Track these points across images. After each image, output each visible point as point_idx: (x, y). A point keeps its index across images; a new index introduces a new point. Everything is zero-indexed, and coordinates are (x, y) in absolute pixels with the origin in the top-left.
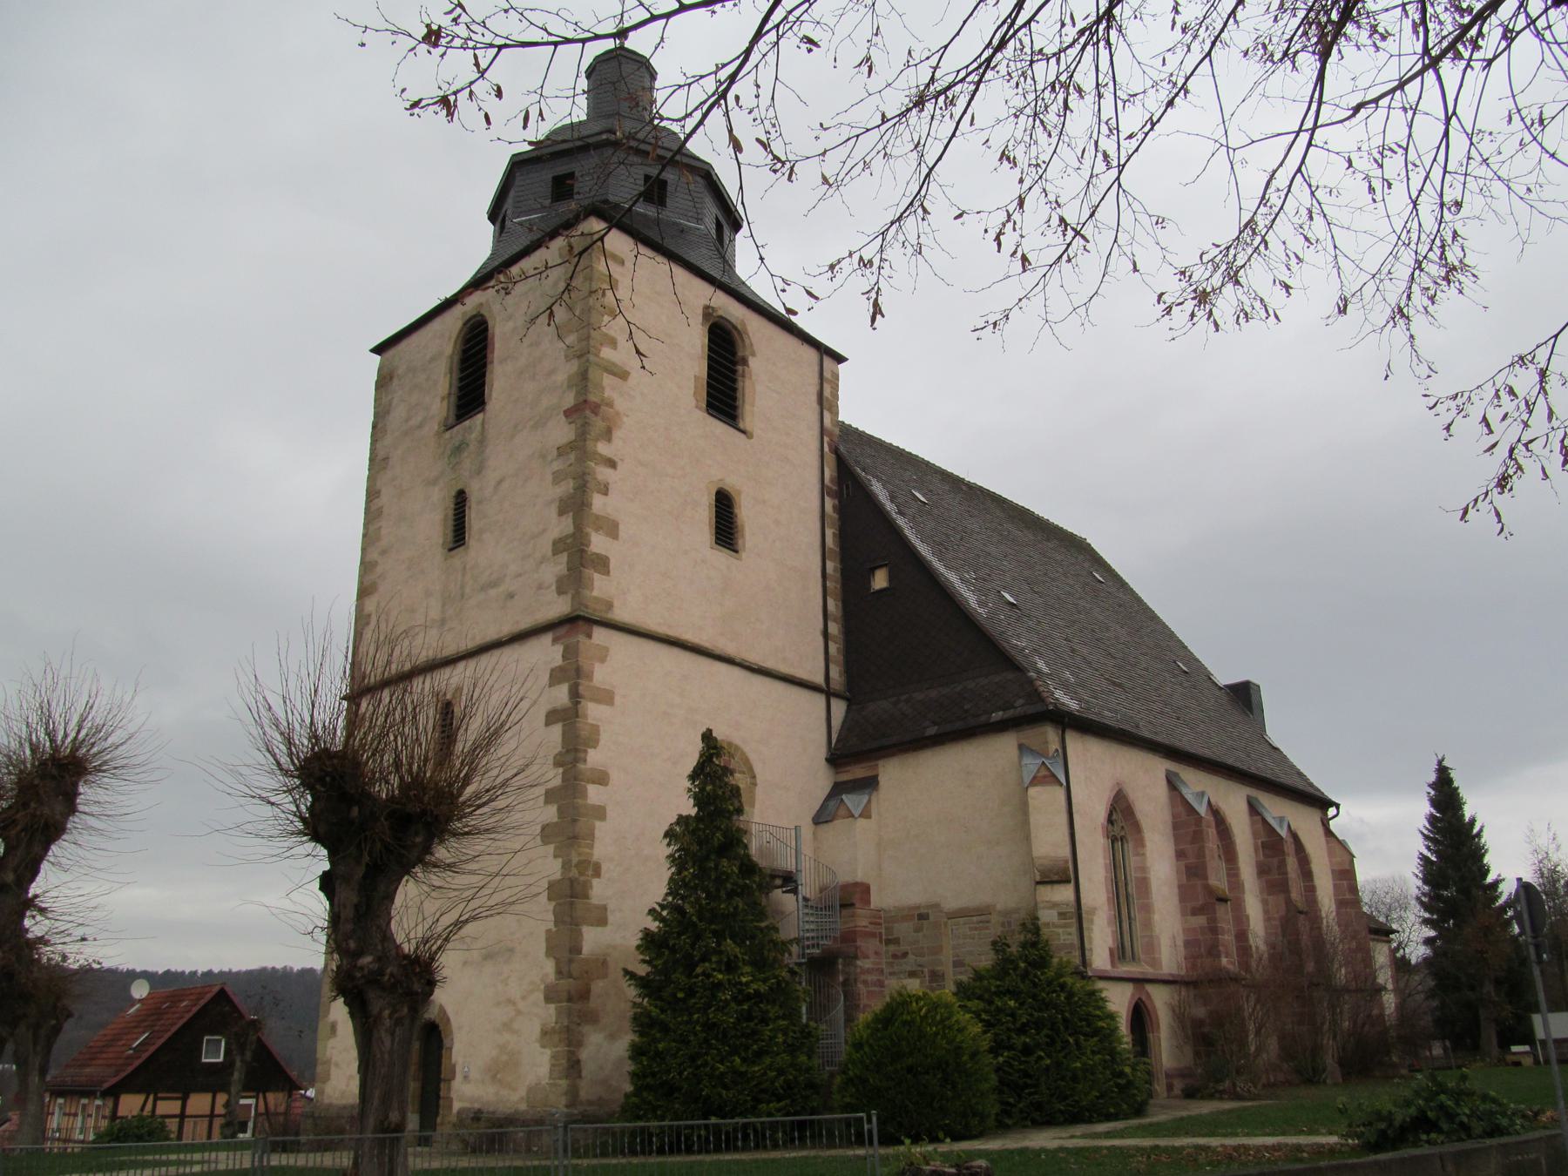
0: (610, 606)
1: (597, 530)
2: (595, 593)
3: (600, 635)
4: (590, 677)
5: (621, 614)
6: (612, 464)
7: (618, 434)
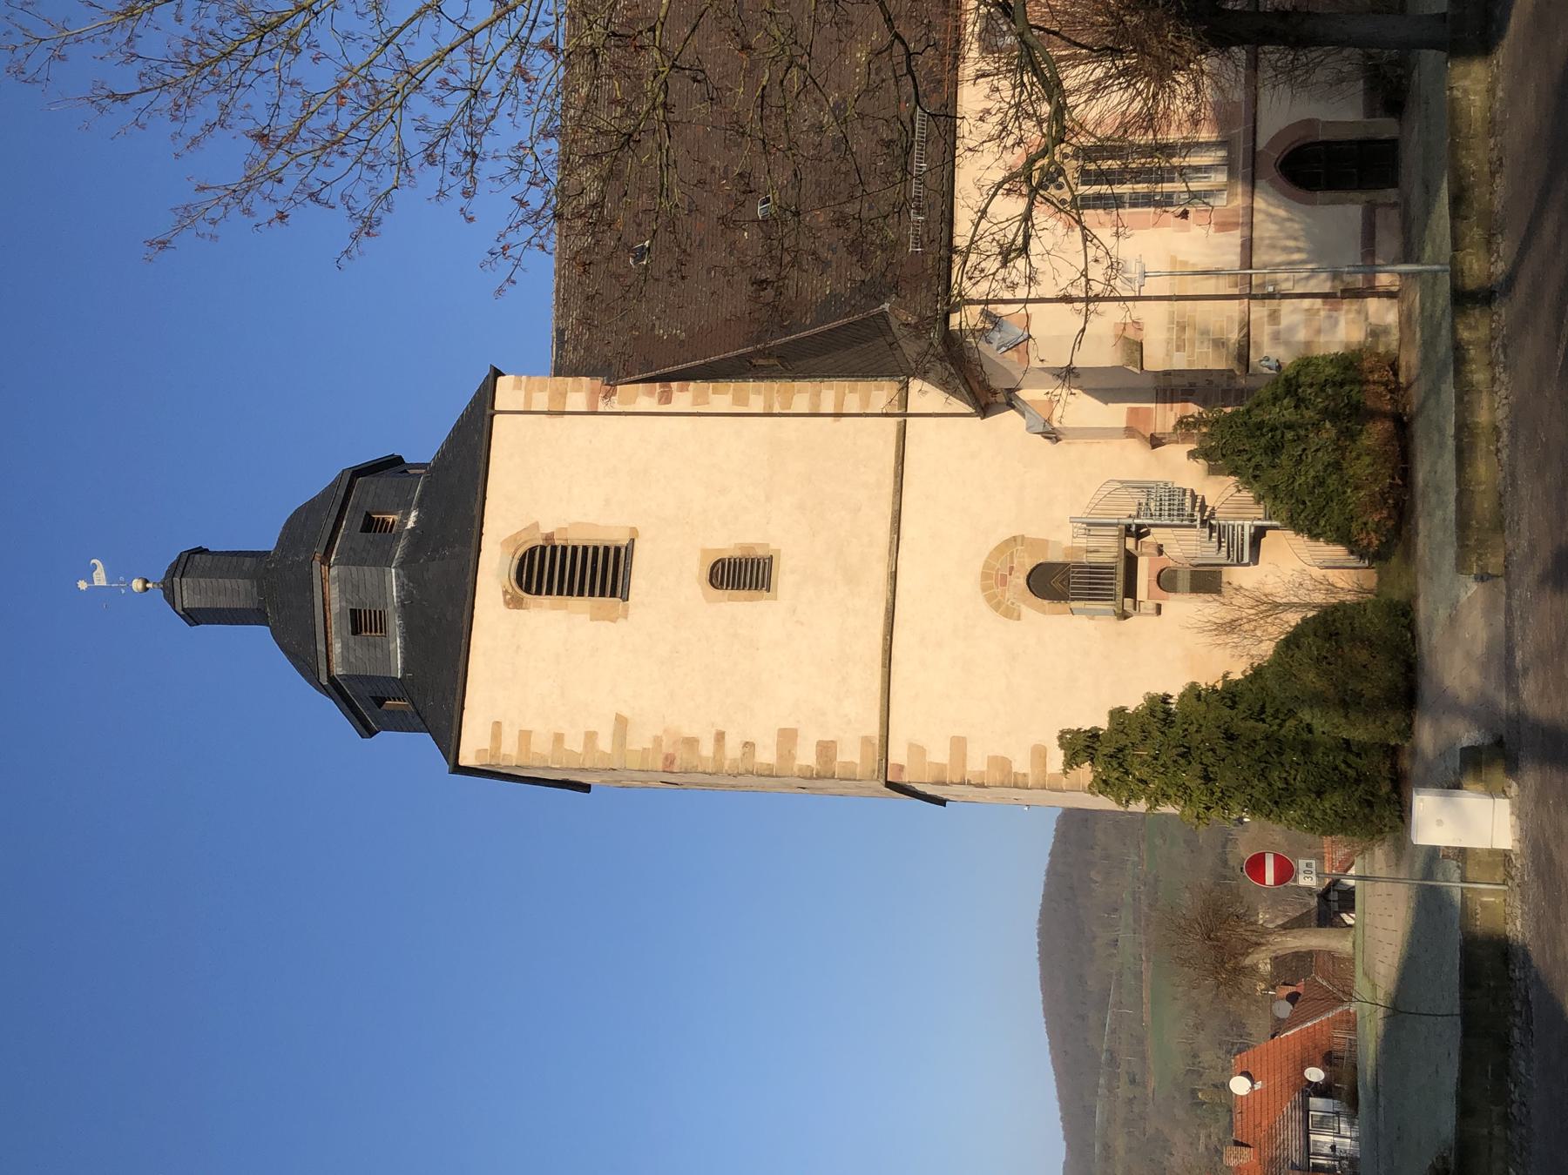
0: (866, 741)
1: (794, 758)
2: (858, 761)
3: (897, 755)
4: (942, 767)
5: (874, 730)
6: (720, 737)
7: (687, 732)
